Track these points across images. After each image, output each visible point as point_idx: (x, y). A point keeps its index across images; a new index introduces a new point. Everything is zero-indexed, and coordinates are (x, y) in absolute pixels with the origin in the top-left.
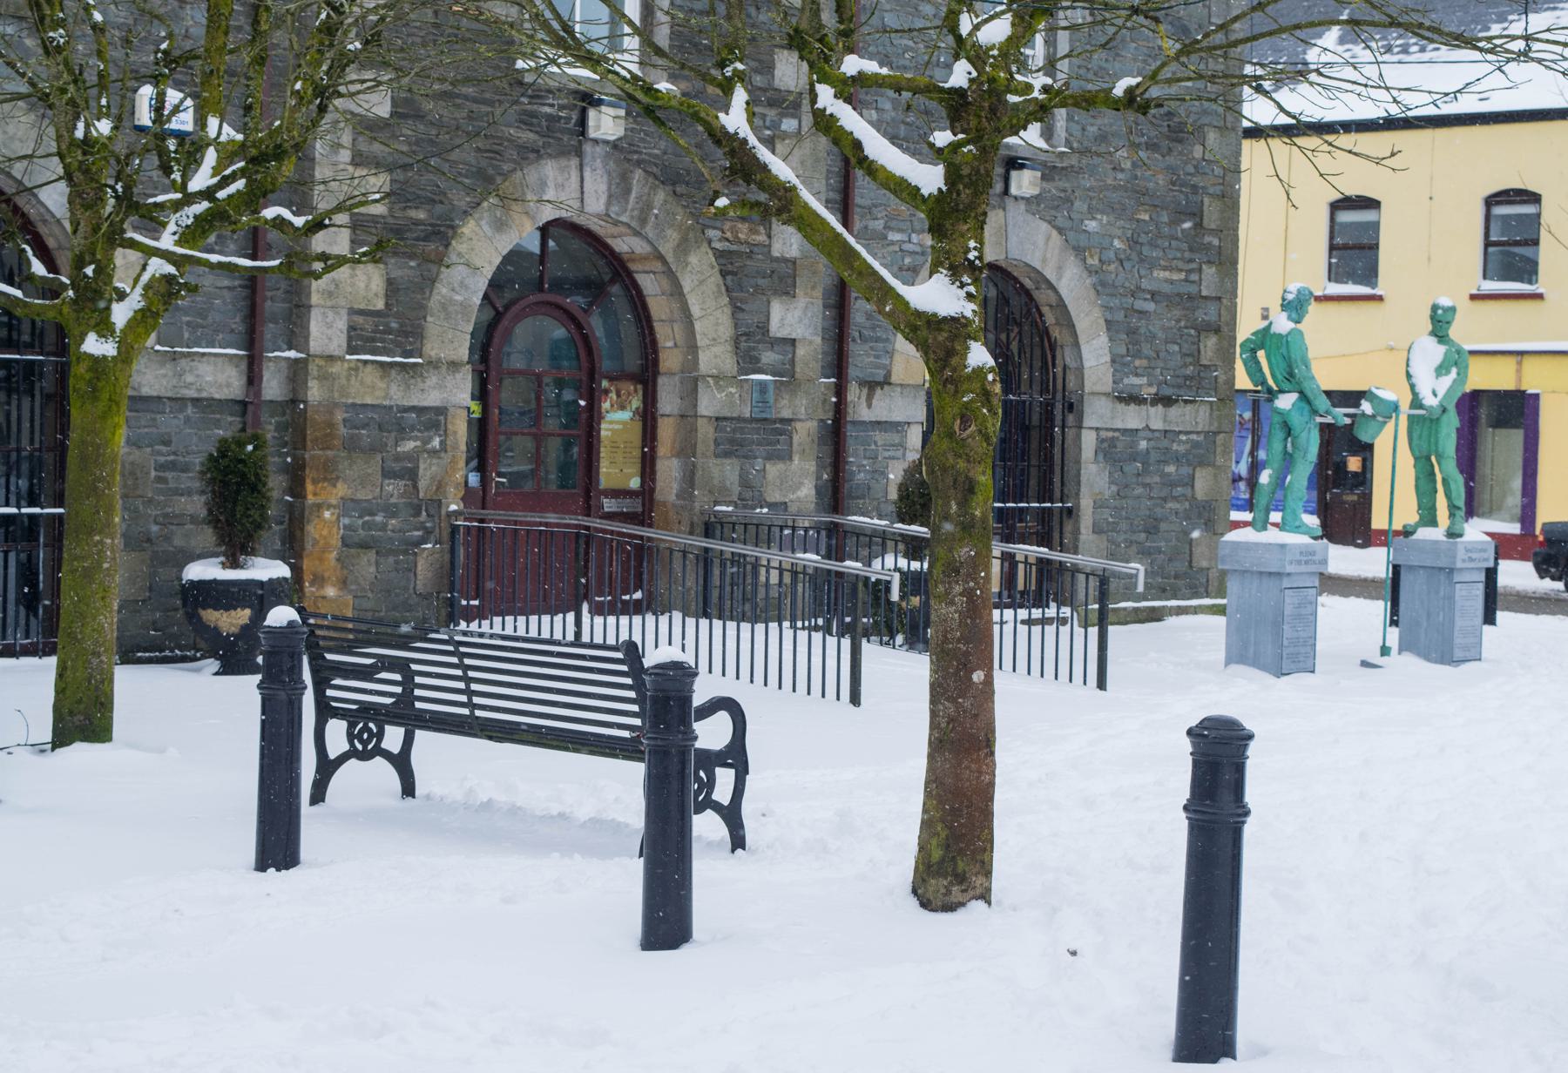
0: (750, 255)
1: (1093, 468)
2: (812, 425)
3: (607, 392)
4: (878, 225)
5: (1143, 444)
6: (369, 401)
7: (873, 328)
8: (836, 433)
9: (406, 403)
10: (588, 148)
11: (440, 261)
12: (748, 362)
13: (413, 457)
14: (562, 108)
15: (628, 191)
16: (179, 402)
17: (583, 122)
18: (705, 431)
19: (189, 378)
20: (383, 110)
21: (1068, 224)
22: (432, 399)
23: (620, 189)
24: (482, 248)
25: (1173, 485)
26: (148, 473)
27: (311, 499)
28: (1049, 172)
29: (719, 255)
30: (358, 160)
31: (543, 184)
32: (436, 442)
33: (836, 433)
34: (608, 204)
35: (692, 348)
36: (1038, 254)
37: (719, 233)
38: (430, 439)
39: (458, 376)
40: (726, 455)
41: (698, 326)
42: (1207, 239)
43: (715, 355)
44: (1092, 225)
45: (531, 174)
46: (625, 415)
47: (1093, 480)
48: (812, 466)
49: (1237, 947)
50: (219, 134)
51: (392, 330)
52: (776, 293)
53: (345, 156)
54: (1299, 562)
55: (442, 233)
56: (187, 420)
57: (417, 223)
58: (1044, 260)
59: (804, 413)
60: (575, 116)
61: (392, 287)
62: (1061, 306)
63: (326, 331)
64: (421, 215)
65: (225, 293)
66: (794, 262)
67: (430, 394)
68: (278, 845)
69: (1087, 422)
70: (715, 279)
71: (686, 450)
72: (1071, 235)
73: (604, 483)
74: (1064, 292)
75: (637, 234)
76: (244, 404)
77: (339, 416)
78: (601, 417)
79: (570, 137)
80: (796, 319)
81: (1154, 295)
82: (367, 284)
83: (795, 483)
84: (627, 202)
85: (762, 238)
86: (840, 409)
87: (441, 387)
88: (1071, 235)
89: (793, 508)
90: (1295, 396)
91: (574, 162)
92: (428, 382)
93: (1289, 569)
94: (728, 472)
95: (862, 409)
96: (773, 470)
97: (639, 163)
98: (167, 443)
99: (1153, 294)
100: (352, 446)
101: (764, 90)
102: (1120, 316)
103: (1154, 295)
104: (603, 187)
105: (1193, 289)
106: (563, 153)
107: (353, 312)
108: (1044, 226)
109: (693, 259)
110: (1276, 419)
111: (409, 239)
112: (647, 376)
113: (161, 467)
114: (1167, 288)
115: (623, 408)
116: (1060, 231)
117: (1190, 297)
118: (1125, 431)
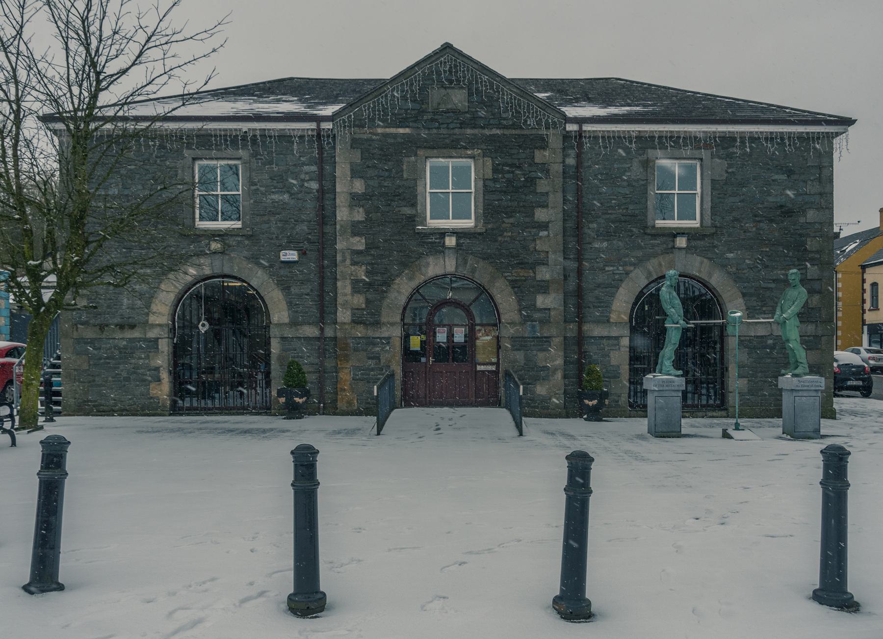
0: (525, 281)
15: (466, 263)
20: (362, 247)
22: (386, 335)
24: (402, 289)
30: (354, 263)
31: (428, 264)
34: (457, 267)
40: (519, 350)
44: (731, 255)
49: (586, 529)
50: (191, 401)
51: (368, 317)
53: (348, 262)
55: (388, 283)
61: (368, 302)
63: (344, 315)
64: (379, 278)
66: (548, 281)
67: (385, 332)
68: (521, 434)
77: (349, 341)
82: (359, 300)
94: (520, 356)
96: (541, 355)
97: (471, 254)
107: (352, 309)
108: (699, 258)
111: (376, 287)
116: (710, 259)
118: (757, 337)
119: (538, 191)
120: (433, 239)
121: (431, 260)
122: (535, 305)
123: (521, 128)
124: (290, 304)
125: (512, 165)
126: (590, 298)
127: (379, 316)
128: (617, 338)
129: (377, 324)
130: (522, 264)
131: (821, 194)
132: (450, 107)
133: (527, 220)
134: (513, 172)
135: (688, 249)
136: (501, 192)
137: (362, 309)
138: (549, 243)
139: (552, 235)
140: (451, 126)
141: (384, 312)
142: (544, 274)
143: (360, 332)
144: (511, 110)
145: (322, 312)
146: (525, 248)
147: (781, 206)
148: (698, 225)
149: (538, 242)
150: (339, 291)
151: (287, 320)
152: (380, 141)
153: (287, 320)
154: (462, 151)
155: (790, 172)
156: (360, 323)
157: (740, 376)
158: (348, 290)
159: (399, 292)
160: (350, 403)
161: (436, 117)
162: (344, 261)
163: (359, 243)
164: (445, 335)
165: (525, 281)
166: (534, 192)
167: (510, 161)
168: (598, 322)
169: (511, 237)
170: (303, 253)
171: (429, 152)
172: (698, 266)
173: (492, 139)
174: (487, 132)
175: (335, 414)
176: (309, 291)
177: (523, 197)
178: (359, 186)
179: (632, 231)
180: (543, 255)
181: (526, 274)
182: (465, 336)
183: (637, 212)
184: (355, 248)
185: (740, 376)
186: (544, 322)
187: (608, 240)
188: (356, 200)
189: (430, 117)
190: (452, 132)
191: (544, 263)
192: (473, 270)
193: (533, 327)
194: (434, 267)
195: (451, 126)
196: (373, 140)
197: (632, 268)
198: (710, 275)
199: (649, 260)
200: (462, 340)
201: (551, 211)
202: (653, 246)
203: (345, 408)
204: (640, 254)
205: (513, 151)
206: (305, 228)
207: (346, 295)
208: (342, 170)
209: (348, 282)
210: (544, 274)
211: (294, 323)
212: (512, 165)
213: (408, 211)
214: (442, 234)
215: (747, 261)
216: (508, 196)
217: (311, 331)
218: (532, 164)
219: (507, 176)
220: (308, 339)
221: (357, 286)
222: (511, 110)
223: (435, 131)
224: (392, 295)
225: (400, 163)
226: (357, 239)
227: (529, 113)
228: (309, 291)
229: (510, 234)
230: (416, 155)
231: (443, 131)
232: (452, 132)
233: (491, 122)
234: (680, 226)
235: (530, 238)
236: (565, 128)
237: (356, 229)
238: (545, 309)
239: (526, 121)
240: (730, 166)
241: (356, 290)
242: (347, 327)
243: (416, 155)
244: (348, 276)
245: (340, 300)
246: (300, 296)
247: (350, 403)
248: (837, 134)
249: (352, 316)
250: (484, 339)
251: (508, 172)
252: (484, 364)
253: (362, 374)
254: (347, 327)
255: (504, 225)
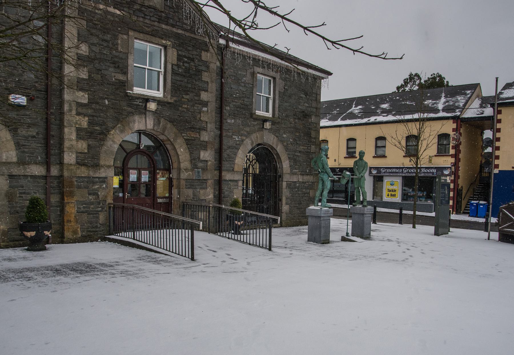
0: (194, 140)
1: (285, 190)
2: (212, 181)
3: (158, 173)
4: (231, 134)
5: (298, 185)
6: (83, 175)
7: (229, 158)
8: (219, 182)
9: (94, 176)
10: (147, 113)
11: (103, 140)
12: (195, 166)
13: (98, 190)
14: (140, 102)
15: (159, 124)
16: (26, 176)
17: (146, 106)
18: (183, 183)
19: (28, 170)
20: (86, 101)
21: (279, 135)
22: (103, 175)
23: (157, 122)
25: (305, 194)
26: (16, 195)
27: (66, 201)
28: (273, 123)
29: (186, 140)
30: (78, 114)
31: (134, 121)
32: (104, 186)
33: (219, 182)
34: (154, 126)
35: (179, 163)
36: (272, 142)
37: (185, 135)
38: (103, 185)
39: (110, 169)
40: (189, 188)
41: (180, 157)
42: (312, 140)
43: (185, 164)
44: (285, 136)
45: (131, 119)
46: (164, 179)
47: (285, 193)
48: (212, 191)
51: (90, 160)
52: (202, 149)
53: (74, 112)
54: (325, 214)
56: (28, 181)
57: (96, 130)
58: (273, 143)
59: (210, 177)
60: (144, 105)
62: (277, 154)
63: (69, 158)
65: (40, 148)
67: (102, 173)
69: (284, 180)
70: (185, 146)
71: (179, 188)
72: (280, 138)
73: (158, 195)
74: (278, 151)
75: (163, 134)
76: (46, 177)
77: (74, 179)
78: (157, 179)
79: (143, 111)
80: (207, 155)
81: (300, 152)
82: (82, 146)
83: (208, 195)
84: (159, 126)
85: (198, 136)
86: (220, 176)
87: (106, 172)
88: (280, 138)
89: (207, 200)
90: (453, 160)
91: (143, 116)
92: (101, 171)
93: (322, 215)
94: (190, 192)
95: (227, 176)
96: (202, 192)
97: (162, 117)
98: (23, 187)
99: (300, 151)
100: (79, 187)
101: (198, 100)
102: (292, 156)
103: (300, 152)
104: (152, 123)
105: (309, 151)
106: (141, 113)
107: (77, 153)
108: (273, 136)
109: (178, 141)
110: (320, 178)
112: (168, 169)
113: (21, 193)
114: (303, 150)
115: (163, 177)
116: (277, 137)
117: (308, 152)
118: (293, 182)
119: (203, 79)
120: (138, 102)
121: (137, 118)
122: (199, 158)
123: (195, 34)
124: (18, 145)
125: (189, 58)
126: (225, 155)
127: (99, 159)
128: (237, 181)
129: (97, 166)
130: (192, 129)
131: (316, 108)
132: (151, 4)
133: (196, 98)
134: (189, 63)
135: (270, 130)
136: (182, 75)
137: (86, 153)
138: (208, 115)
139: (209, 111)
140: (152, 19)
141: (102, 156)
142: (205, 137)
143: (83, 172)
144: (190, 18)
145: (48, 154)
146: (195, 118)
147: (303, 112)
148: (271, 116)
149: (202, 114)
150: (66, 137)
151: (15, 159)
152: (101, 15)
153: (15, 159)
154: (157, 40)
155: (306, 94)
156: (84, 165)
157: (287, 204)
158: (74, 137)
159: (113, 141)
160: (75, 232)
161: (143, 9)
162: (70, 110)
163: (83, 97)
164: (136, 176)
165: (194, 140)
166: (200, 79)
167: (187, 55)
168: (228, 171)
169: (186, 108)
170: (30, 100)
171: (137, 35)
172: (270, 139)
173: (177, 36)
174: (174, 30)
175: (62, 242)
176: (35, 134)
177: (194, 81)
178: (84, 49)
179: (245, 115)
180: (204, 125)
181: (194, 136)
182: (149, 178)
183: (248, 103)
184: (79, 101)
185: (287, 204)
186: (205, 169)
187: (234, 119)
188: (81, 61)
189: (139, 7)
190: (153, 23)
191: (205, 129)
192: (164, 129)
193: (198, 172)
194: (140, 123)
195: (152, 19)
196: (96, 13)
197: (245, 138)
198: (277, 146)
199: (252, 134)
200: (147, 180)
201: (210, 95)
202: (254, 126)
203: (71, 237)
204: (248, 129)
205: (190, 48)
206: (33, 76)
207: (71, 140)
208: (71, 30)
209: (73, 129)
210: (205, 137)
211: (21, 162)
212: (189, 58)
213: (121, 77)
214: (147, 100)
215: (291, 140)
216: (184, 78)
217: (38, 170)
218: (200, 60)
219: (186, 65)
220: (34, 177)
221: (81, 134)
222: (190, 18)
223: (141, 19)
224: (109, 143)
225: (116, 37)
226: (81, 94)
227: (200, 24)
228: (35, 134)
229: (186, 106)
230: (127, 34)
231: (147, 21)
232: (153, 23)
233: (178, 24)
234: (264, 115)
235: (198, 111)
236: (218, 41)
237: (80, 85)
238: (205, 161)
239: (198, 30)
240: (285, 85)
241: (79, 137)
242: (73, 167)
243: (127, 34)
244: (74, 123)
245: (67, 144)
246: (26, 138)
247: (75, 232)
248: (323, 78)
249: (77, 159)
250: (161, 180)
251: (186, 62)
252: (162, 198)
253: (84, 208)
254: (73, 167)
255: (183, 100)
